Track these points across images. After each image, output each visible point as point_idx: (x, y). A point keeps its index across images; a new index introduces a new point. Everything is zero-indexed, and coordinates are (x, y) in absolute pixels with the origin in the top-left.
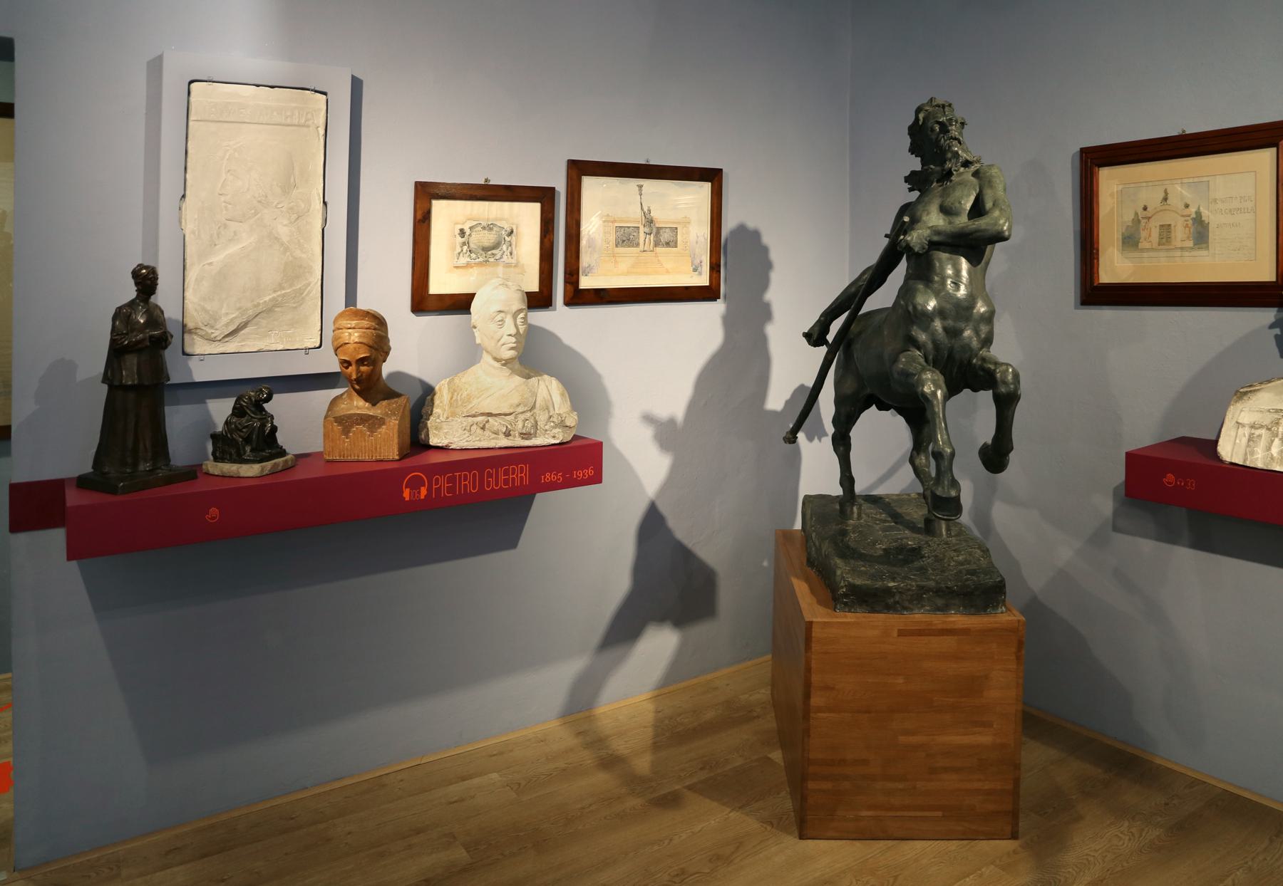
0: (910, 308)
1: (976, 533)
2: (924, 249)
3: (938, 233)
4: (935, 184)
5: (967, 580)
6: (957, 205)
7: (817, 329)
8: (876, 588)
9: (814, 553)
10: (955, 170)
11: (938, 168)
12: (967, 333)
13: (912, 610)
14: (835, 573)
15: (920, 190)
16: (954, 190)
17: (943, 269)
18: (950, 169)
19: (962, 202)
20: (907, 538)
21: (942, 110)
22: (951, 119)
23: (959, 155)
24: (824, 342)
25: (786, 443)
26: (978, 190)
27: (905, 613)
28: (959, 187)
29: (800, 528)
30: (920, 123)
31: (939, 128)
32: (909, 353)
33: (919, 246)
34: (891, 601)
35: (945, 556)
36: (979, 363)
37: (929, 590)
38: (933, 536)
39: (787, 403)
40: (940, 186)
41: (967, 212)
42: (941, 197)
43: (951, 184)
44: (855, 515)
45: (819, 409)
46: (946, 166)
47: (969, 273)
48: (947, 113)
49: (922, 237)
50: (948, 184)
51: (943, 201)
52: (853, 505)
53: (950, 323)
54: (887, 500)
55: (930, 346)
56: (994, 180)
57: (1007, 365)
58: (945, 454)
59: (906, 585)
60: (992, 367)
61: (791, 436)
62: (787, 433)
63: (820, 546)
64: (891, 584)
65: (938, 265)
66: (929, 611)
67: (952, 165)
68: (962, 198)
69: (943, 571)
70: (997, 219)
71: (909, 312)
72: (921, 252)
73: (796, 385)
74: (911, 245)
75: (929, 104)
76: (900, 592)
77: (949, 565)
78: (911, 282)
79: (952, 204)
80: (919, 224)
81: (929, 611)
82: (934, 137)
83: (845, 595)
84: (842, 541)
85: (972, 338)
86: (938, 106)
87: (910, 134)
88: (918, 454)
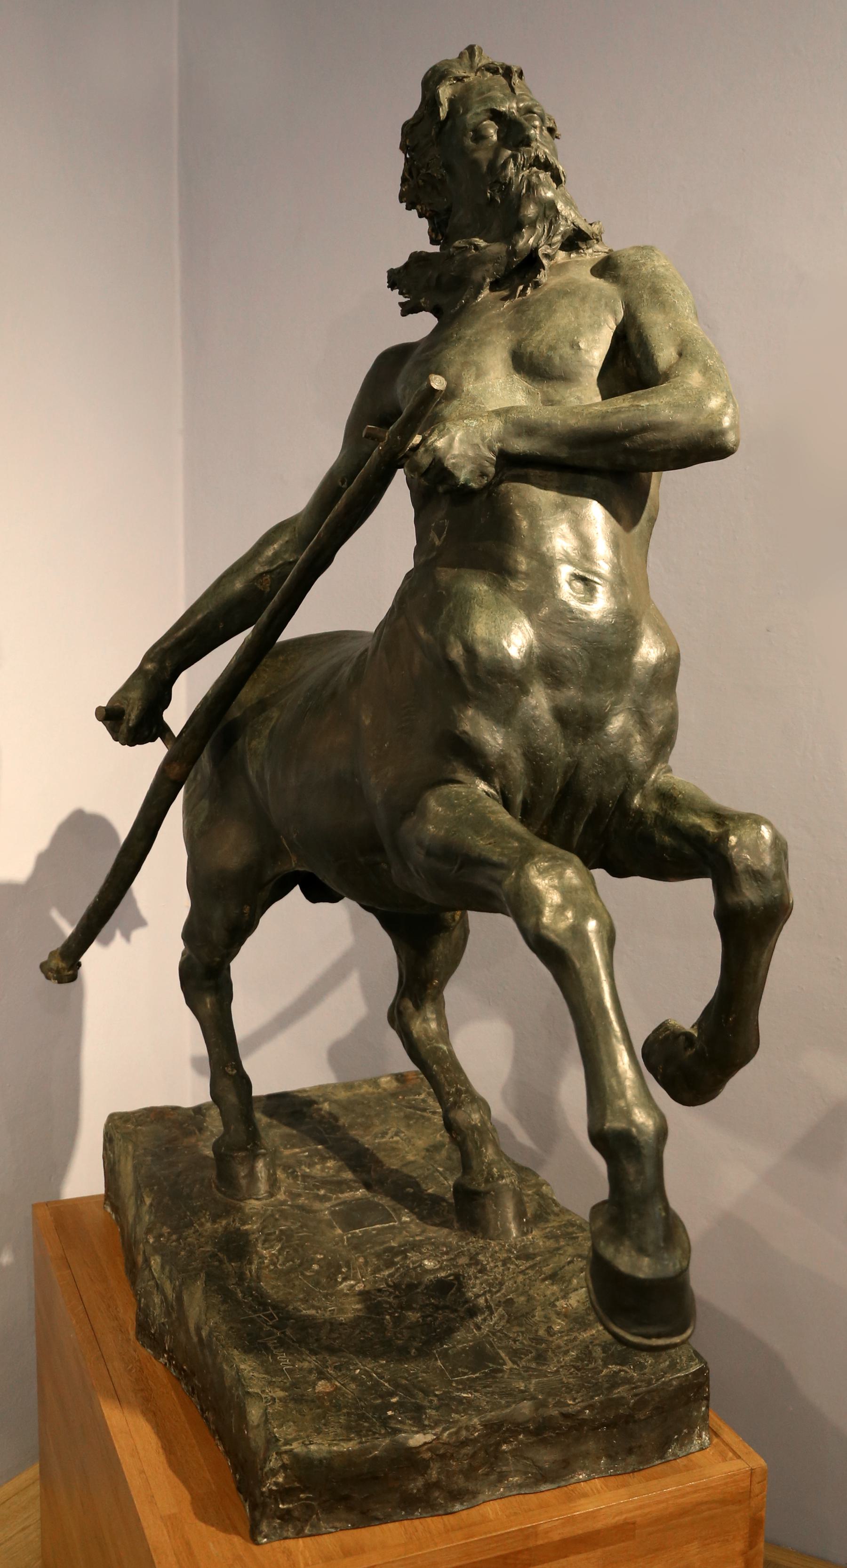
0: (456, 652)
1: (522, 1136)
2: (483, 474)
3: (528, 430)
4: (486, 292)
5: (614, 1381)
6: (566, 350)
7: (135, 695)
8: (375, 1458)
9: (157, 1312)
10: (547, 256)
11: (497, 248)
12: (617, 724)
13: (474, 1494)
14: (243, 1415)
15: (437, 311)
16: (551, 310)
17: (539, 533)
18: (534, 251)
19: (582, 345)
20: (415, 1246)
21: (504, 81)
22: (529, 110)
23: (557, 212)
24: (161, 731)
25: (48, 978)
26: (621, 315)
27: (458, 1507)
28: (565, 302)
29: (98, 1187)
30: (443, 113)
31: (499, 133)
32: (455, 788)
33: (469, 467)
34: (416, 1485)
35: (530, 1299)
36: (654, 807)
37: (516, 1428)
38: (486, 1235)
39: (44, 860)
40: (505, 299)
41: (596, 373)
42: (510, 328)
43: (539, 294)
44: (263, 1187)
45: (131, 894)
46: (521, 243)
47: (616, 546)
48: (518, 92)
49: (477, 440)
50: (529, 291)
51: (519, 343)
52: (255, 1157)
53: (571, 694)
54: (326, 1106)
55: (518, 765)
56: (666, 285)
57: (758, 821)
58: (642, 1139)
59: (457, 1433)
60: (710, 827)
61: (62, 965)
62: (52, 954)
63: (179, 1299)
64: (418, 1439)
65: (524, 524)
66: (520, 1486)
67: (539, 239)
68: (578, 332)
69: (540, 1358)
70: (700, 399)
71: (451, 666)
72: (473, 485)
73: (62, 814)
74: (449, 462)
75: (466, 60)
76: (442, 1457)
77: (549, 1330)
78: (444, 575)
79: (552, 348)
80: (456, 403)
81: (520, 1486)
82: (483, 156)
83: (284, 1493)
84: (241, 1277)
85: (631, 735)
86: (492, 69)
87: (404, 147)
88: (418, 1007)
